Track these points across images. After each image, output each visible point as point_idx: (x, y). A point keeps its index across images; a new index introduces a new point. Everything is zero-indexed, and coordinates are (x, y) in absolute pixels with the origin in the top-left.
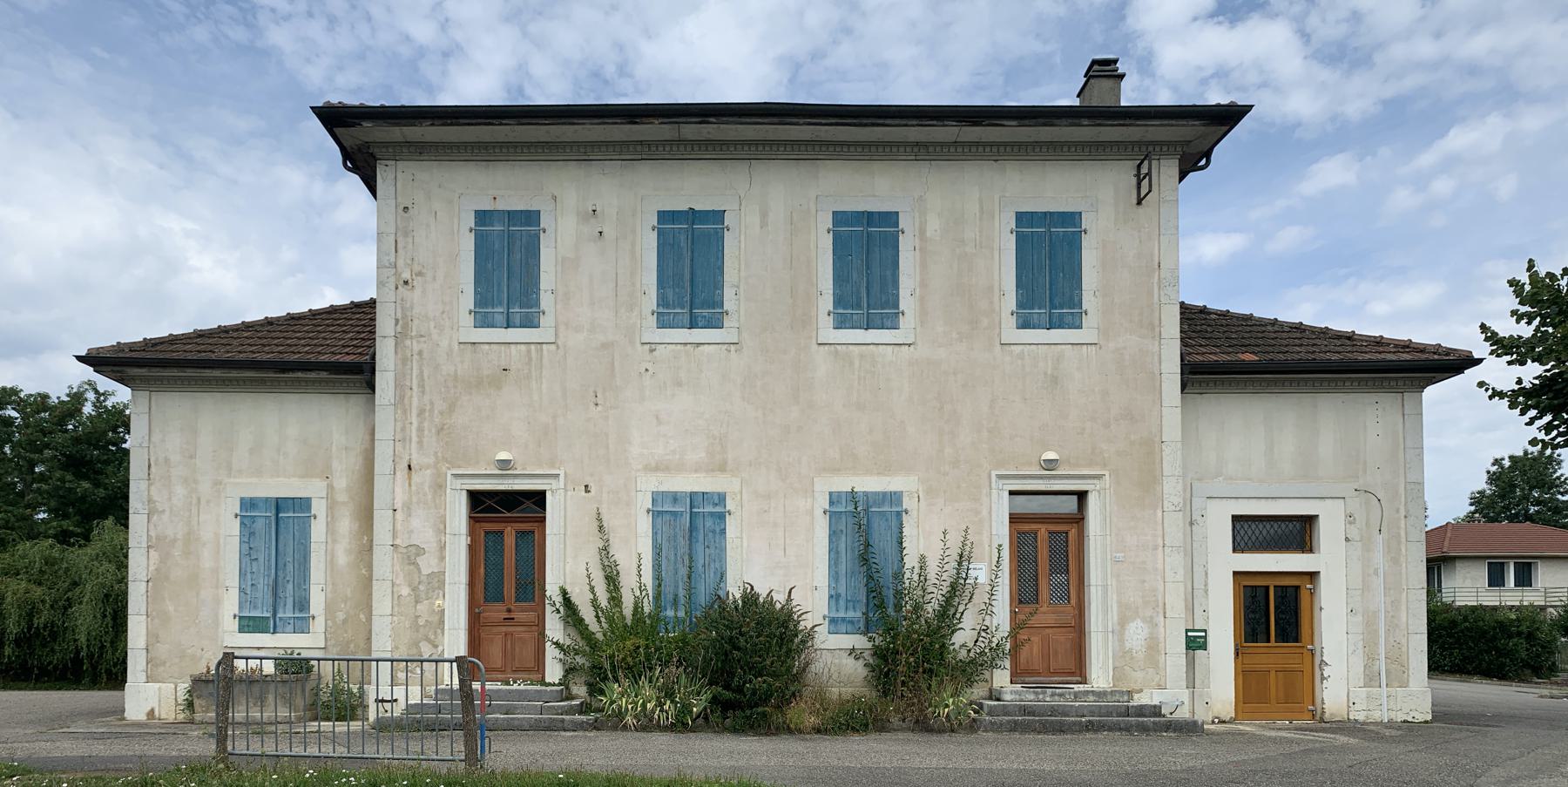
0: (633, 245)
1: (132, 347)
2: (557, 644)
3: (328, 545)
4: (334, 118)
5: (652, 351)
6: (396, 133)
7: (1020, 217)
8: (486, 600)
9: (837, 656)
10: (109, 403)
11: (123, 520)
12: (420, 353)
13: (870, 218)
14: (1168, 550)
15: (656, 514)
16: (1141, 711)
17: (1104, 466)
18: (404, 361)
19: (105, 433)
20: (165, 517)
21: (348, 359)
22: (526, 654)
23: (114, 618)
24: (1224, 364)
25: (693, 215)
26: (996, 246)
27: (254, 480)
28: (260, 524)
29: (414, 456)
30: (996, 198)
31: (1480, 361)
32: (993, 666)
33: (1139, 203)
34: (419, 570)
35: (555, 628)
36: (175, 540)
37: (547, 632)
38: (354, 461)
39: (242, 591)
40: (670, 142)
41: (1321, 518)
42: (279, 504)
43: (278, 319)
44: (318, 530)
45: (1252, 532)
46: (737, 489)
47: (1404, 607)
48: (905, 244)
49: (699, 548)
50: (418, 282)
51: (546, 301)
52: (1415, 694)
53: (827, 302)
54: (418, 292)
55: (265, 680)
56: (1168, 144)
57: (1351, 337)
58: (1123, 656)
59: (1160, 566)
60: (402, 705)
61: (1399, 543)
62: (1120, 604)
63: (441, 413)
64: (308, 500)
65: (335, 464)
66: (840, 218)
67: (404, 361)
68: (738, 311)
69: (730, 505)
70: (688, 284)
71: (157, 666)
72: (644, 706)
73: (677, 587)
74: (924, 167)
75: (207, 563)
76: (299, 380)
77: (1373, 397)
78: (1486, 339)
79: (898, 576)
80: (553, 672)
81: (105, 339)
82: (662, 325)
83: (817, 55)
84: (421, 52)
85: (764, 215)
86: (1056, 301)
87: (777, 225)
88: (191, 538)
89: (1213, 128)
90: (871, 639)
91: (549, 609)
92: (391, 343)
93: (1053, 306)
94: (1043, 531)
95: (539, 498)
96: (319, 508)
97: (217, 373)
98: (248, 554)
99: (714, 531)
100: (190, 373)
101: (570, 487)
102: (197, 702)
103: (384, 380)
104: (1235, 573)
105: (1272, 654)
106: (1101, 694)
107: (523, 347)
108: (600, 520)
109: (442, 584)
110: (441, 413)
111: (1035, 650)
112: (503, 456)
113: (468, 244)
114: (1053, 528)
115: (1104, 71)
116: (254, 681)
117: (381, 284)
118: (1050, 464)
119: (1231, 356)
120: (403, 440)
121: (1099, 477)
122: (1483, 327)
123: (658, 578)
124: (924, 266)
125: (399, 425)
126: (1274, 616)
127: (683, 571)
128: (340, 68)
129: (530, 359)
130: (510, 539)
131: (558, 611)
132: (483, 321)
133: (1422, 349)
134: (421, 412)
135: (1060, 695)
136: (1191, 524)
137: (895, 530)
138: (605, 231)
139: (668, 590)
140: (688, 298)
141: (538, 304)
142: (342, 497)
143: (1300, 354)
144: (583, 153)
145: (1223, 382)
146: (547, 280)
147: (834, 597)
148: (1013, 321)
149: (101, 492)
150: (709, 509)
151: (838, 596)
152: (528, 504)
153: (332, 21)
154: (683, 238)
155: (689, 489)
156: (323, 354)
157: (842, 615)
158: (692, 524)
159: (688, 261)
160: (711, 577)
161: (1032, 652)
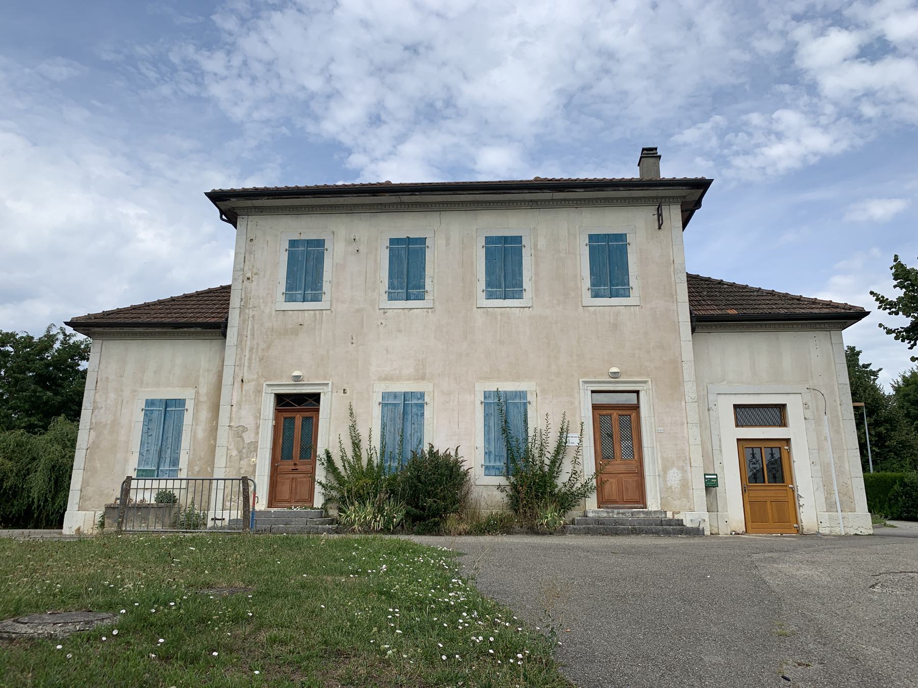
0: (376, 255)
1: (96, 316)
2: (320, 483)
3: (193, 427)
4: (216, 197)
5: (385, 313)
7: (591, 237)
8: (282, 458)
9: (487, 488)
10: (71, 342)
11: (75, 415)
12: (253, 317)
14: (690, 425)
15: (384, 405)
16: (670, 522)
17: (648, 376)
18: (244, 321)
20: (102, 411)
21: (213, 320)
24: (718, 315)
25: (409, 241)
28: (155, 414)
29: (246, 374)
31: (869, 313)
32: (584, 495)
33: (660, 228)
34: (243, 441)
35: (321, 474)
36: (106, 425)
38: (212, 378)
39: (141, 454)
41: (788, 407)
42: (167, 403)
43: (178, 297)
44: (188, 418)
45: (745, 414)
46: (431, 390)
47: (846, 461)
48: (526, 253)
49: (409, 424)
50: (255, 278)
51: (326, 287)
52: (860, 519)
53: (482, 285)
54: (255, 283)
55: (148, 507)
57: (799, 299)
58: (666, 490)
59: (686, 435)
60: (227, 519)
61: (839, 421)
62: (662, 458)
63: (263, 350)
65: (201, 380)
66: (489, 240)
67: (244, 321)
69: (427, 399)
70: (405, 277)
71: (85, 500)
72: (365, 517)
73: (394, 448)
74: (536, 213)
76: (185, 333)
80: (319, 501)
81: (81, 312)
82: (390, 299)
83: (585, 88)
84: (312, 96)
85: (448, 239)
87: (455, 246)
88: (115, 424)
89: (693, 191)
90: (508, 479)
91: (318, 463)
92: (237, 311)
94: (615, 414)
95: (316, 397)
96: (190, 405)
98: (147, 432)
99: (417, 415)
100: (126, 330)
101: (335, 390)
102: (107, 521)
103: (232, 332)
104: (738, 440)
105: (767, 491)
106: (650, 512)
108: (351, 410)
109: (256, 450)
110: (263, 350)
112: (296, 373)
113: (284, 257)
114: (621, 412)
115: (650, 154)
116: (142, 507)
117: (234, 279)
118: (615, 375)
119: (721, 308)
122: (872, 293)
123: (383, 446)
124: (537, 264)
125: (238, 356)
126: (767, 469)
127: (398, 438)
128: (257, 108)
130: (298, 422)
131: (323, 464)
132: (290, 298)
133: (837, 306)
134: (251, 350)
135: (623, 514)
136: (709, 410)
138: (361, 249)
139: (389, 450)
141: (321, 288)
142: (203, 398)
143: (765, 309)
144: (350, 209)
146: (327, 275)
147: (488, 454)
149: (59, 398)
150: (415, 401)
152: (310, 400)
153: (254, 79)
154: (403, 252)
155: (403, 391)
156: (198, 317)
157: (492, 464)
158: (405, 410)
159: (406, 265)
161: (611, 488)
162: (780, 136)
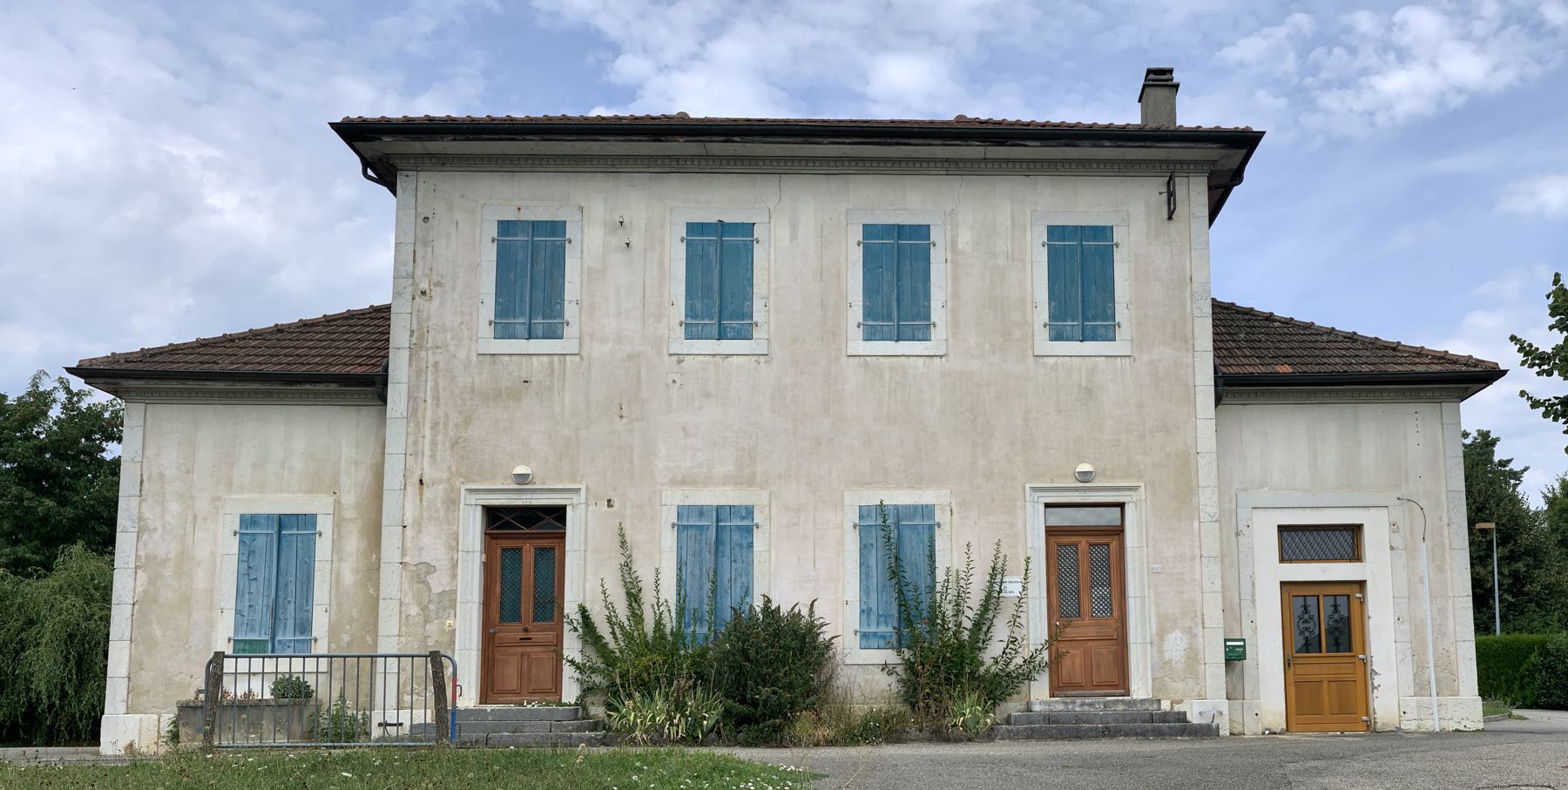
0: (662, 255)
1: (128, 358)
3: (333, 565)
4: (353, 132)
5: (679, 362)
6: (417, 147)
8: (502, 619)
9: (865, 669)
10: (83, 405)
11: (105, 542)
12: (436, 364)
13: (900, 230)
14: (1205, 561)
15: (681, 529)
16: (1165, 717)
17: (1140, 477)
18: (419, 373)
19: (77, 441)
20: (157, 536)
21: (359, 370)
22: (544, 674)
23: (79, 664)
25: (722, 227)
26: (1028, 258)
27: (256, 496)
28: (261, 541)
29: (427, 470)
30: (1028, 212)
33: (1170, 218)
35: (572, 647)
36: (165, 561)
37: (565, 653)
38: (364, 475)
39: (238, 612)
40: (699, 157)
42: (282, 521)
44: (323, 548)
45: (1297, 541)
47: (1451, 615)
48: (937, 256)
49: (726, 562)
50: (436, 292)
51: (570, 311)
52: (1464, 706)
53: (857, 314)
54: (436, 303)
55: (260, 705)
56: (1195, 162)
57: (1395, 348)
58: (1162, 668)
59: (1198, 576)
62: (1159, 616)
63: (457, 426)
64: (314, 516)
65: (344, 479)
66: (869, 231)
67: (419, 373)
68: (768, 322)
69: (758, 518)
70: (716, 295)
72: (654, 718)
75: (201, 583)
76: (307, 392)
77: (1409, 408)
78: (1520, 350)
79: (932, 588)
80: (570, 692)
81: (98, 349)
85: (794, 228)
86: (1089, 314)
87: (806, 239)
88: (184, 559)
89: (1230, 152)
90: (899, 653)
91: (567, 627)
92: (405, 354)
93: (1085, 318)
94: (1083, 542)
95: (559, 513)
96: (324, 525)
97: (220, 385)
98: (246, 574)
99: (741, 546)
100: (191, 385)
101: (592, 502)
102: (183, 731)
104: (1282, 583)
105: (1323, 666)
107: (545, 359)
110: (457, 426)
111: (1077, 662)
112: (521, 469)
118: (1085, 477)
119: (1267, 362)
120: (416, 454)
121: (1135, 489)
125: (411, 438)
126: (1326, 630)
127: (708, 586)
129: (553, 370)
130: (528, 555)
131: (576, 629)
132: (503, 332)
133: (1455, 360)
134: (435, 425)
135: (1090, 705)
137: (926, 538)
138: (634, 241)
139: (692, 604)
140: (716, 309)
141: (561, 315)
142: (349, 513)
143: (1337, 365)
144: (611, 165)
145: (1263, 393)
147: (865, 612)
148: (1046, 333)
149: (69, 512)
151: (870, 610)
152: (549, 519)
154: (712, 249)
156: (333, 363)
157: (873, 629)
158: (719, 537)
160: (738, 591)
161: (1073, 664)
162: (1403, 56)
